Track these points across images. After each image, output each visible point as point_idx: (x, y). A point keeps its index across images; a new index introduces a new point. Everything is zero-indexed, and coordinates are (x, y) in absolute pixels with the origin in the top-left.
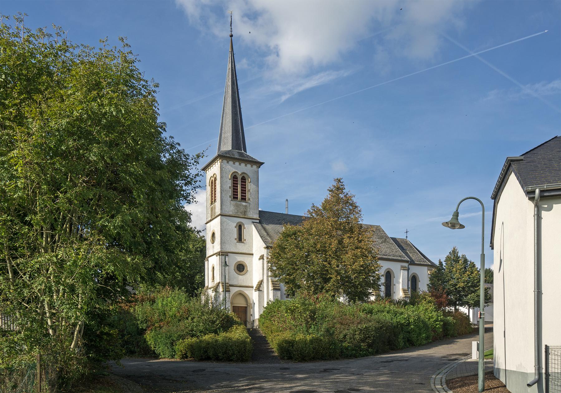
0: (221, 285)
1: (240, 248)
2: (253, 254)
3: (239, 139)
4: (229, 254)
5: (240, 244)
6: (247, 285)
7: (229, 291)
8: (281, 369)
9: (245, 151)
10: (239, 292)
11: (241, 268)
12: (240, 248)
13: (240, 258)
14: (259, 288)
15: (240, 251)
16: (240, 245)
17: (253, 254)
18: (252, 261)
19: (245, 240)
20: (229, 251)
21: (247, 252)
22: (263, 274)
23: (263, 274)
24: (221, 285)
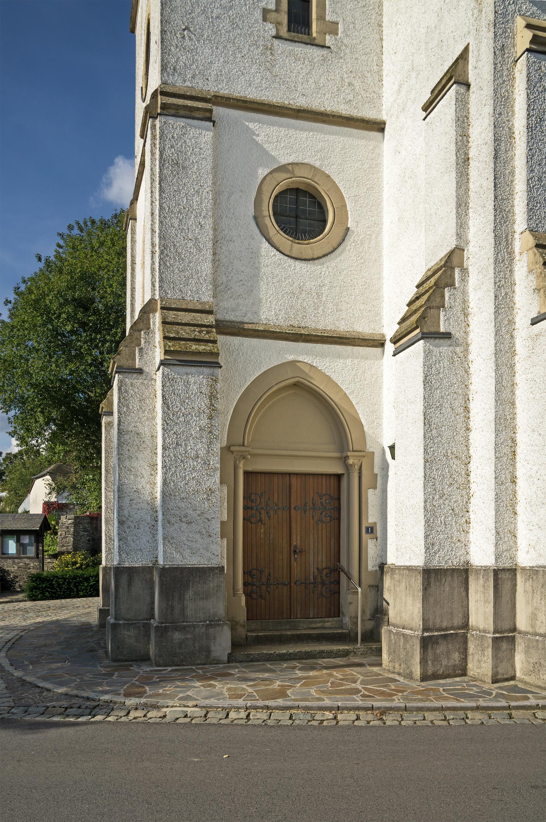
0: (156, 319)
1: (299, 75)
2: (379, 127)
3: (333, 634)
4: (219, 111)
5: (299, 49)
6: (342, 327)
7: (210, 362)
8: (37, 637)
9: (339, 562)
10: (289, 377)
11: (302, 212)
12: (299, 75)
13: (288, 146)
14: (429, 316)
15: (301, 102)
16: (294, 57)
17: (379, 127)
18: (375, 166)
19: (333, 28)
20: (224, 90)
21: (344, 110)
22: (462, 205)
23: (462, 205)
24: (156, 319)
